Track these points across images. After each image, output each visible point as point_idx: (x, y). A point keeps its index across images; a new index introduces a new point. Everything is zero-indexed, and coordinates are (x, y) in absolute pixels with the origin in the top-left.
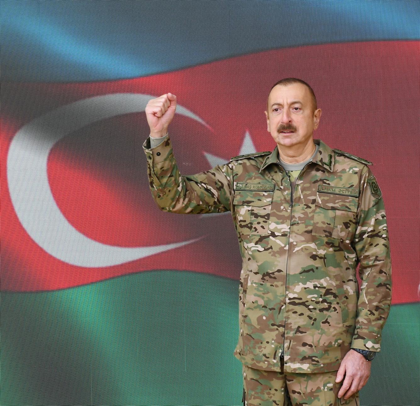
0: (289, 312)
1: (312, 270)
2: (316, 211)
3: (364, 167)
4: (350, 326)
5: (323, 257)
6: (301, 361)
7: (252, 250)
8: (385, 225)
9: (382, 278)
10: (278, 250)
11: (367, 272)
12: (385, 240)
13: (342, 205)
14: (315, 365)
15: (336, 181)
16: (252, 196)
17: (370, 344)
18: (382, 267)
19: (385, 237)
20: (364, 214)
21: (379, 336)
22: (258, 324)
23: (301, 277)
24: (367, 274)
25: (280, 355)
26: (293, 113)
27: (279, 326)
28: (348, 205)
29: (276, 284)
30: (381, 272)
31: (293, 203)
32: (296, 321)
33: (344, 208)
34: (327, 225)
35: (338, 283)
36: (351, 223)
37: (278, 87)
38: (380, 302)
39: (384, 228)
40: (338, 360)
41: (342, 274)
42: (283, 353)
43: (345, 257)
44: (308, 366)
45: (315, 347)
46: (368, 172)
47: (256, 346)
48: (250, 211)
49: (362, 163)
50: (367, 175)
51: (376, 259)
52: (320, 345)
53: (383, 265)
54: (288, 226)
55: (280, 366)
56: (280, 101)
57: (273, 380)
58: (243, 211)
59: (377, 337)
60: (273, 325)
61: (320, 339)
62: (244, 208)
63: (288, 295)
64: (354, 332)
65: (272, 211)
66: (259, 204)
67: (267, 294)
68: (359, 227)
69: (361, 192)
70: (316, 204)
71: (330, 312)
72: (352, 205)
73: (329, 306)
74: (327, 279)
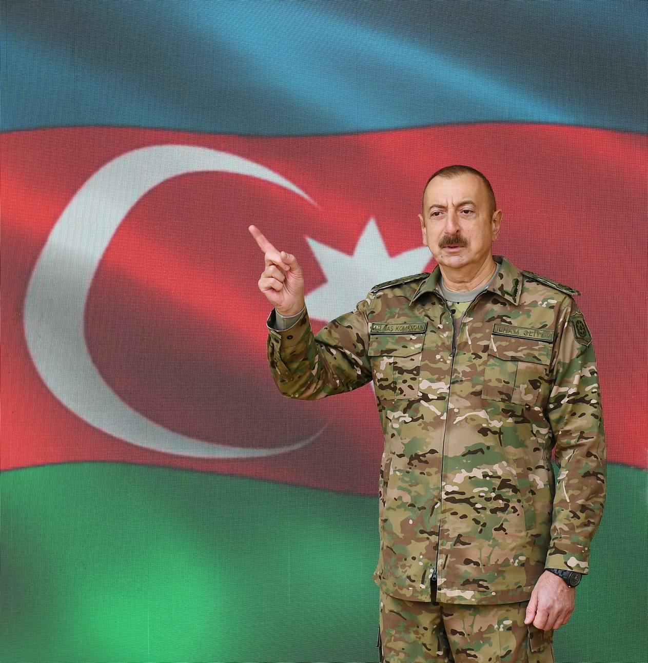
0: (445, 513)
1: (481, 450)
2: (488, 363)
3: (565, 298)
4: (537, 536)
6: (462, 587)
8: (596, 385)
9: (591, 464)
10: (432, 421)
11: (567, 455)
12: (596, 407)
13: (528, 355)
14: (482, 593)
15: (520, 318)
17: (573, 562)
18: (590, 448)
19: (595, 404)
20: (563, 368)
21: (586, 549)
23: (465, 461)
24: (567, 458)
25: (430, 576)
26: (463, 218)
27: (431, 534)
28: (536, 354)
29: (428, 471)
30: (589, 454)
31: (456, 350)
32: (455, 526)
33: (531, 359)
35: (520, 470)
36: (541, 381)
37: (438, 179)
38: (587, 500)
39: (594, 390)
40: (520, 587)
41: (527, 458)
42: (435, 574)
43: (532, 431)
46: (570, 305)
47: (398, 564)
48: (393, 364)
49: (562, 292)
50: (569, 310)
51: (582, 436)
52: (491, 563)
53: (594, 445)
54: (446, 385)
55: (430, 593)
56: (442, 201)
57: (421, 613)
59: (583, 551)
60: (422, 532)
61: (491, 554)
62: (383, 360)
64: (549, 544)
66: (404, 352)
67: (415, 486)
68: (555, 387)
69: (559, 335)
70: (489, 353)
71: (507, 514)
72: (544, 355)
74: (503, 464)
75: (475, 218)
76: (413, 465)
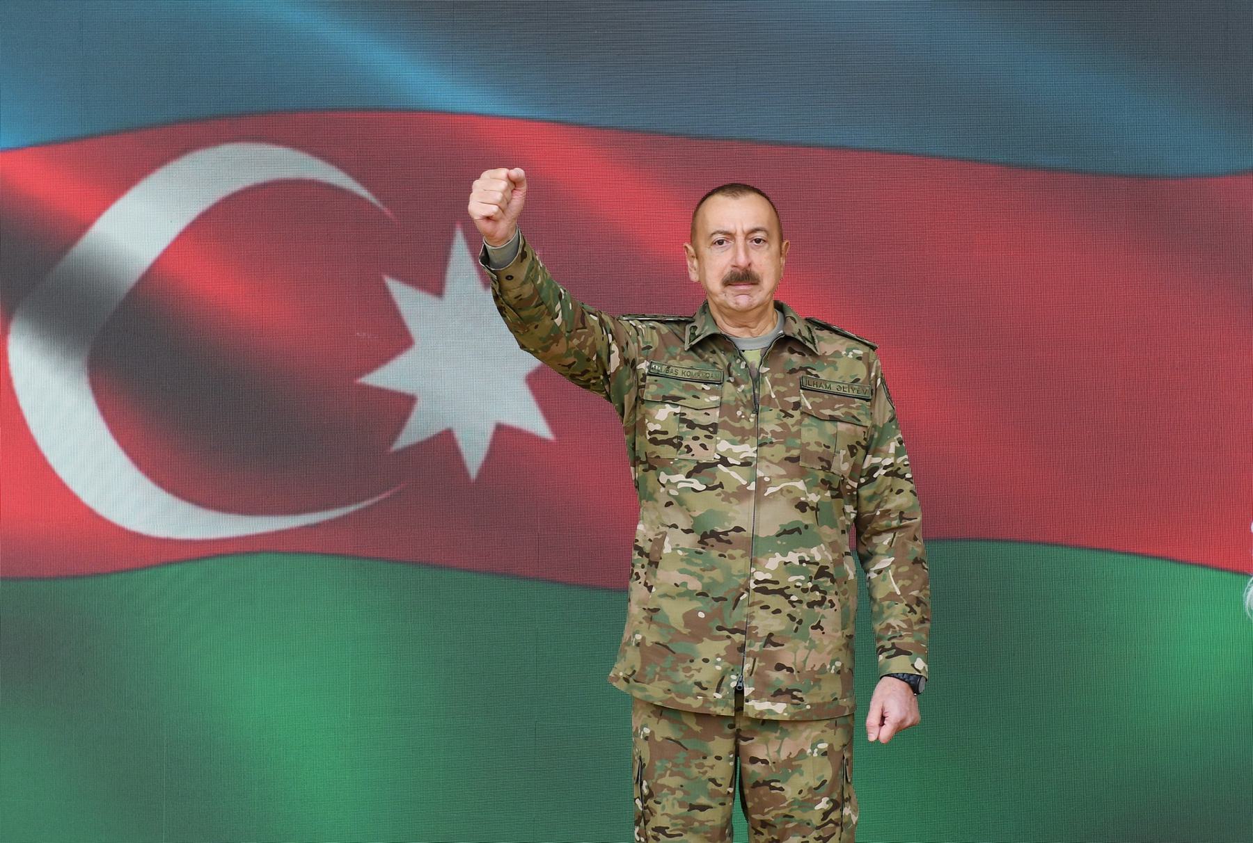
1: (798, 530)
2: (803, 423)
5: (815, 507)
6: (773, 698)
7: (678, 488)
8: (906, 457)
10: (735, 490)
13: (847, 414)
16: (681, 388)
22: (687, 625)
23: (779, 542)
26: (753, 248)
27: (734, 631)
28: (855, 413)
32: (765, 623)
34: (823, 447)
36: (858, 447)
40: (836, 699)
42: (741, 682)
44: (784, 708)
45: (798, 672)
48: (678, 416)
54: (752, 447)
56: (729, 227)
58: (662, 416)
60: (720, 628)
61: (807, 658)
62: (665, 408)
63: (753, 575)
65: (722, 419)
67: (711, 570)
68: (869, 457)
71: (825, 609)
73: (822, 597)
74: (821, 547)
75: (768, 249)
76: (708, 545)
